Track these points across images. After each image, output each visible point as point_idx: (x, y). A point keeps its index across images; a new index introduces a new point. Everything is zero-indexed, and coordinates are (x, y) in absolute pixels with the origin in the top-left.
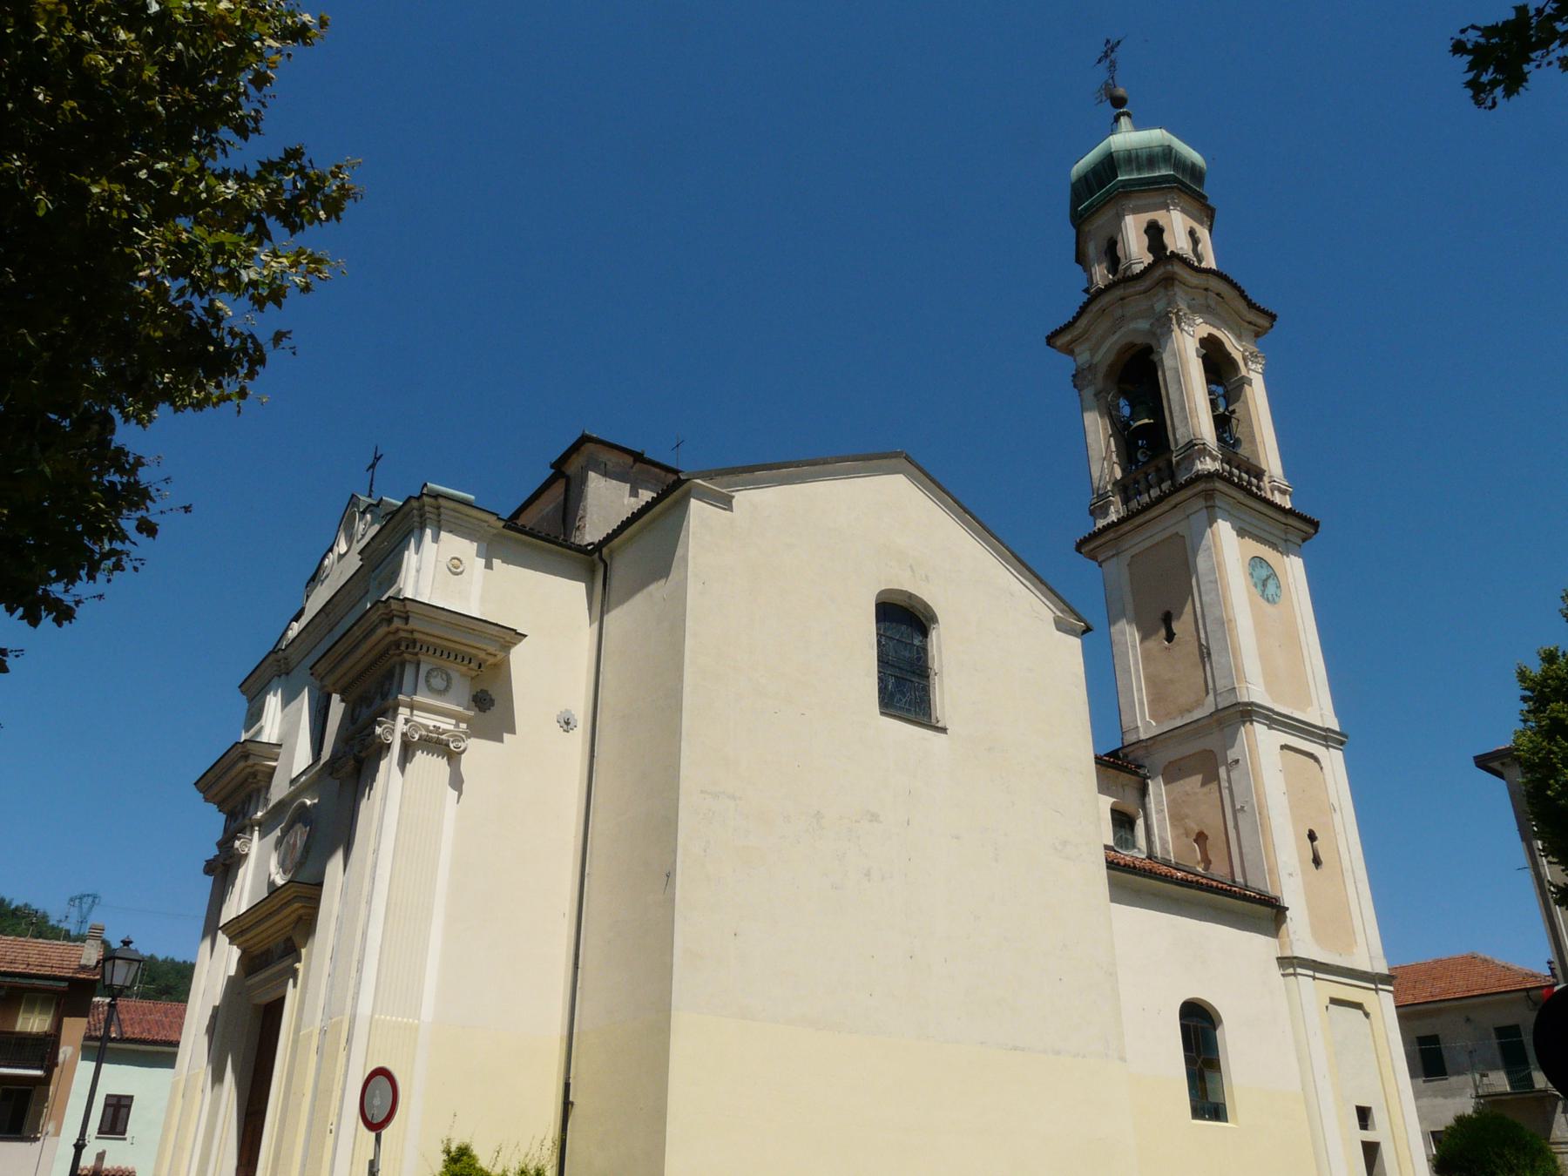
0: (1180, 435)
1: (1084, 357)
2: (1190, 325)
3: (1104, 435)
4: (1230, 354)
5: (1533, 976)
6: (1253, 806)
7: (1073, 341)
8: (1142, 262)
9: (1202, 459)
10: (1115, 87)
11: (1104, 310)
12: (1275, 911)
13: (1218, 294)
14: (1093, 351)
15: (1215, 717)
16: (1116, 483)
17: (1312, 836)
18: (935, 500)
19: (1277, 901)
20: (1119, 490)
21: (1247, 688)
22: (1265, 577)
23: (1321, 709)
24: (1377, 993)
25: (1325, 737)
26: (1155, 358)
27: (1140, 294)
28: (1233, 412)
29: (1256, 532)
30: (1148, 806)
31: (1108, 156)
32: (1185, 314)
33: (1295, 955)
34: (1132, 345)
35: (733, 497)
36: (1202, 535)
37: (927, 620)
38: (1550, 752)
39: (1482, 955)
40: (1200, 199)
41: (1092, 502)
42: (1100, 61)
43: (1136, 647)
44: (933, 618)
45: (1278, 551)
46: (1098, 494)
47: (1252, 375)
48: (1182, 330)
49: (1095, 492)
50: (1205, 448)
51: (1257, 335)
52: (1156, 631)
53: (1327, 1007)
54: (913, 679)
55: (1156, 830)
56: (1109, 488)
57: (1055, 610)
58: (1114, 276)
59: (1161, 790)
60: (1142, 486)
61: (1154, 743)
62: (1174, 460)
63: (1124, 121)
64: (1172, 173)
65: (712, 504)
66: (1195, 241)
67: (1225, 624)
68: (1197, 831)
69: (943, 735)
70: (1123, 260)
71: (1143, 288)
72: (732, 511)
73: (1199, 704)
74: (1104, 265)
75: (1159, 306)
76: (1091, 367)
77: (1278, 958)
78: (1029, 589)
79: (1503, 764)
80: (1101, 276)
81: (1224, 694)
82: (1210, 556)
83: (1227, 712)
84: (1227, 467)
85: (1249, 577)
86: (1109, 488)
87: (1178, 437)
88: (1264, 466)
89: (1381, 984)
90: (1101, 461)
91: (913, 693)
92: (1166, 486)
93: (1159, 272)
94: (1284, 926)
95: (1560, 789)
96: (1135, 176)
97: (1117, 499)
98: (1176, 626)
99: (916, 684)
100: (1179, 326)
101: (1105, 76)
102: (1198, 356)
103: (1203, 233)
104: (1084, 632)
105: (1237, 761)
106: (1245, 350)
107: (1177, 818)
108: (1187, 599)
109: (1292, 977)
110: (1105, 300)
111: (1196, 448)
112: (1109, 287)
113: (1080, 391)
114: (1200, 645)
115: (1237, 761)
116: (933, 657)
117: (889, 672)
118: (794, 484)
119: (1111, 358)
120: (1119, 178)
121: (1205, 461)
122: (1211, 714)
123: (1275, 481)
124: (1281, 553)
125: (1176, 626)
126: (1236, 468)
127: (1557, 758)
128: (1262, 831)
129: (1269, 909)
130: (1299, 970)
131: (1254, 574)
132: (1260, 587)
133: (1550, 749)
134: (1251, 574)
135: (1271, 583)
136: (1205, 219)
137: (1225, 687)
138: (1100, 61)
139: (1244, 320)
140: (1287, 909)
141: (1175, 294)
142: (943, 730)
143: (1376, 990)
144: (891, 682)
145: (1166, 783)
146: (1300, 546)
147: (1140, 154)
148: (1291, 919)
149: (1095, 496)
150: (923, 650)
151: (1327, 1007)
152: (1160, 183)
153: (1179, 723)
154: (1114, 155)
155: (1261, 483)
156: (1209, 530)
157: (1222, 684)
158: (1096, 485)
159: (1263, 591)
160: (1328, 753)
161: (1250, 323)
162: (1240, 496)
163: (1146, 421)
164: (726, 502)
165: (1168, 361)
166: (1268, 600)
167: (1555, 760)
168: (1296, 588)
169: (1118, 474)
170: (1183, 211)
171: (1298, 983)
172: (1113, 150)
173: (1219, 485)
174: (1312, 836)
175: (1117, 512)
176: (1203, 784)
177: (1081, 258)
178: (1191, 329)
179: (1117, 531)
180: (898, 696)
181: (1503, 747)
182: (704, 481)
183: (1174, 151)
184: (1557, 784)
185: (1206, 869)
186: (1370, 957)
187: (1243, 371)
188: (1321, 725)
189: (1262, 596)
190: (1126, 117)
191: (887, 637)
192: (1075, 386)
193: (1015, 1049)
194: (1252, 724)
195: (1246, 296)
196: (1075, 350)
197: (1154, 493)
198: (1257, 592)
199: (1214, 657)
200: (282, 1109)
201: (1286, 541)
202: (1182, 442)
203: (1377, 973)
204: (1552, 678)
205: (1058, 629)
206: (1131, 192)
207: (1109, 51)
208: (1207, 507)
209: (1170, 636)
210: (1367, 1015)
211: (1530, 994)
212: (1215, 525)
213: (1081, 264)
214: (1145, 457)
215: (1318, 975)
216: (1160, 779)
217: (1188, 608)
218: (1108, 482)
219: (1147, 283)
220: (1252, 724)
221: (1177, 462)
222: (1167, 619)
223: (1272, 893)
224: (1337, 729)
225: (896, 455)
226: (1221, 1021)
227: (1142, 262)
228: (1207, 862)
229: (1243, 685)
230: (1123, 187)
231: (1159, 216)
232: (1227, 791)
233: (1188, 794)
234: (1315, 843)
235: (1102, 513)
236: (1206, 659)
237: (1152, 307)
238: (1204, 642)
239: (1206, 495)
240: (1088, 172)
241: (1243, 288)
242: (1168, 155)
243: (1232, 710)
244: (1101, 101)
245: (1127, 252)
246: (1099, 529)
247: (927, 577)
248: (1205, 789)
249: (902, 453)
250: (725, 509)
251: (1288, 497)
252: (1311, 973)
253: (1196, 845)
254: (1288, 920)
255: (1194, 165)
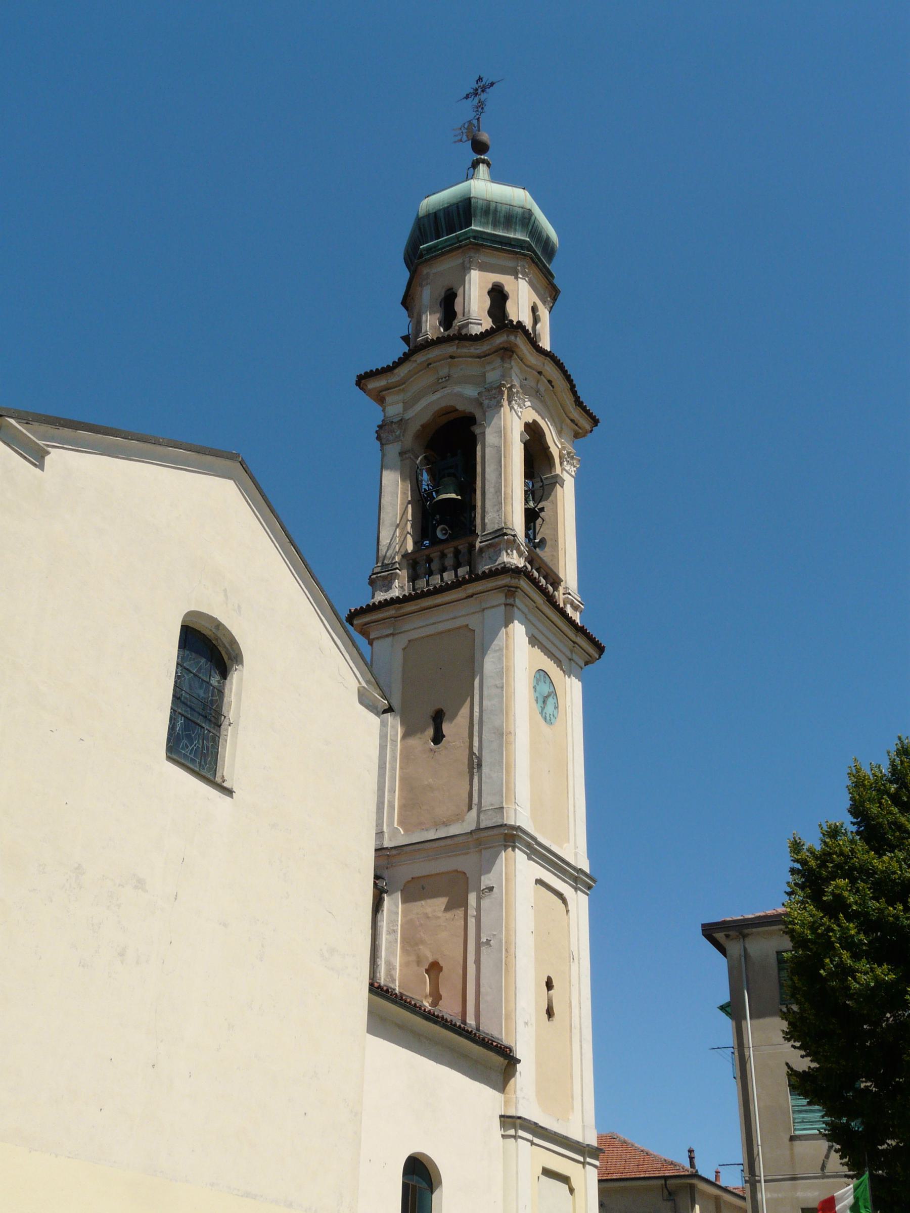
0: (491, 521)
1: (394, 409)
2: (519, 405)
3: (402, 499)
4: (549, 448)
5: (672, 1163)
6: (501, 941)
7: (387, 388)
8: (481, 324)
9: (509, 551)
10: (479, 130)
11: (430, 364)
12: (506, 1061)
13: (550, 382)
14: (407, 406)
15: (475, 837)
16: (405, 556)
17: (549, 985)
18: (262, 520)
19: (511, 1050)
20: (408, 564)
21: (515, 810)
22: (546, 694)
23: (576, 847)
24: (584, 1167)
25: (577, 878)
26: (477, 430)
27: (471, 357)
28: (542, 510)
29: (549, 646)
30: (379, 924)
31: (466, 199)
32: (518, 392)
33: (519, 1115)
34: (450, 410)
35: (48, 453)
36: (495, 633)
37: (230, 658)
38: (830, 929)
39: (622, 1136)
40: (548, 275)
41: (376, 571)
42: (467, 97)
43: (396, 741)
44: (237, 658)
45: (562, 669)
46: (383, 563)
47: (565, 476)
48: (512, 408)
49: (381, 559)
50: (514, 541)
51: (576, 436)
52: (423, 730)
53: (538, 1177)
54: (204, 725)
55: (383, 953)
56: (397, 559)
57: (361, 679)
58: (445, 330)
59: (398, 907)
60: (449, 561)
61: (399, 854)
62: (478, 545)
63: (482, 168)
64: (528, 239)
65: (21, 455)
66: (536, 320)
67: (502, 735)
68: (431, 960)
69: (228, 799)
70: (460, 316)
71: (478, 352)
72: (43, 470)
73: (459, 818)
74: (438, 315)
75: (492, 376)
76: (402, 423)
77: (501, 1116)
78: (339, 649)
79: (727, 936)
80: (432, 326)
81: (490, 813)
82: (500, 659)
83: (490, 833)
84: (529, 567)
85: (532, 690)
86: (397, 559)
87: (486, 521)
88: (561, 576)
89: (591, 1157)
90: (394, 528)
91: (201, 742)
92: (463, 571)
93: (500, 340)
94: (512, 1081)
95: (833, 969)
96: (489, 231)
97: (403, 574)
98: (447, 728)
99: (206, 732)
100: (510, 402)
101: (471, 115)
102: (521, 441)
103: (544, 313)
104: (385, 712)
105: (491, 889)
106: (564, 448)
107: (410, 942)
108: (465, 701)
109: (513, 1139)
110: (433, 353)
111: (506, 537)
112: (439, 341)
113: (382, 445)
114: (471, 753)
115: (491, 889)
116: (230, 704)
117: (180, 711)
118: (117, 457)
119: (425, 418)
120: (473, 227)
121: (512, 554)
122: (471, 833)
123: (569, 594)
124: (564, 672)
125: (446, 728)
126: (537, 570)
127: (835, 936)
128: (507, 969)
129: (502, 1059)
130: (521, 1133)
131: (538, 688)
132: (541, 700)
133: (829, 926)
134: (535, 688)
135: (551, 701)
136: (549, 299)
137: (492, 805)
138: (467, 97)
139: (568, 417)
140: (519, 1061)
141: (512, 368)
142: (229, 792)
143: (584, 1164)
144: (180, 721)
145: (405, 901)
146: (582, 668)
147: (499, 209)
148: (520, 1073)
149: (379, 564)
150: (221, 693)
151: (538, 1177)
152: (514, 246)
153: (431, 835)
154: (473, 200)
155: (556, 593)
156: (503, 630)
157: (488, 801)
158: (383, 551)
159: (543, 709)
160: (575, 896)
161: (572, 421)
162: (539, 599)
163: (453, 496)
164: (37, 457)
165: (490, 438)
166: (545, 719)
167: (833, 939)
168: (572, 712)
169: (410, 547)
170: (531, 283)
171: (517, 1146)
172: (471, 196)
173: (524, 583)
174: (549, 985)
175: (402, 588)
176: (447, 909)
177: (407, 301)
178: (520, 410)
179: (400, 608)
180: (185, 741)
181: (731, 919)
182: (18, 423)
183: (533, 218)
184: (832, 964)
185: (435, 1004)
186: (584, 1126)
187: (558, 470)
188: (573, 862)
189: (541, 713)
190: (485, 166)
191: (185, 668)
192: (379, 438)
193: (247, 1195)
194: (513, 850)
195: (576, 392)
196: (387, 399)
197: (449, 576)
198: (537, 708)
199: (485, 770)
200: (816, 1176)
201: (570, 660)
202: (490, 528)
203: (588, 1145)
204: (835, 853)
205: (361, 702)
206: (482, 245)
207: (480, 90)
208: (506, 605)
209: (438, 738)
210: (572, 1190)
211: (668, 1182)
212: (511, 626)
213: (407, 308)
214: (445, 534)
215: (536, 1141)
216: (398, 895)
217: (465, 711)
218: (397, 553)
219: (485, 347)
220: (513, 850)
221: (481, 550)
222: (438, 718)
223: (506, 1041)
224: (588, 871)
225: (231, 457)
226: (440, 1182)
227: (481, 324)
228: (436, 997)
229: (512, 806)
230: (475, 238)
231: (506, 281)
232: (473, 920)
233: (428, 917)
234: (550, 992)
235: (384, 586)
236: (475, 770)
237: (484, 375)
238: (476, 750)
239: (509, 591)
240: (440, 210)
241: (574, 382)
242: (525, 219)
243: (496, 831)
244: (461, 141)
245: (466, 310)
246: (374, 604)
247: (239, 607)
248: (449, 915)
249: (238, 455)
250: (35, 465)
251: (578, 613)
252: (529, 1137)
253: (426, 975)
254: (518, 1073)
255: (548, 238)
